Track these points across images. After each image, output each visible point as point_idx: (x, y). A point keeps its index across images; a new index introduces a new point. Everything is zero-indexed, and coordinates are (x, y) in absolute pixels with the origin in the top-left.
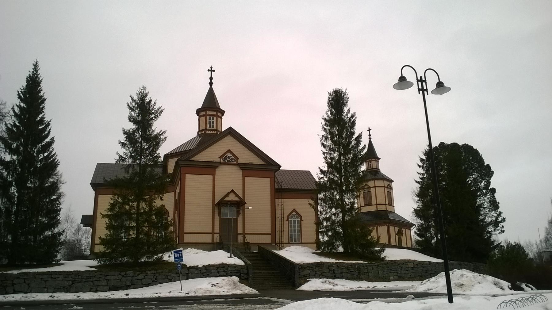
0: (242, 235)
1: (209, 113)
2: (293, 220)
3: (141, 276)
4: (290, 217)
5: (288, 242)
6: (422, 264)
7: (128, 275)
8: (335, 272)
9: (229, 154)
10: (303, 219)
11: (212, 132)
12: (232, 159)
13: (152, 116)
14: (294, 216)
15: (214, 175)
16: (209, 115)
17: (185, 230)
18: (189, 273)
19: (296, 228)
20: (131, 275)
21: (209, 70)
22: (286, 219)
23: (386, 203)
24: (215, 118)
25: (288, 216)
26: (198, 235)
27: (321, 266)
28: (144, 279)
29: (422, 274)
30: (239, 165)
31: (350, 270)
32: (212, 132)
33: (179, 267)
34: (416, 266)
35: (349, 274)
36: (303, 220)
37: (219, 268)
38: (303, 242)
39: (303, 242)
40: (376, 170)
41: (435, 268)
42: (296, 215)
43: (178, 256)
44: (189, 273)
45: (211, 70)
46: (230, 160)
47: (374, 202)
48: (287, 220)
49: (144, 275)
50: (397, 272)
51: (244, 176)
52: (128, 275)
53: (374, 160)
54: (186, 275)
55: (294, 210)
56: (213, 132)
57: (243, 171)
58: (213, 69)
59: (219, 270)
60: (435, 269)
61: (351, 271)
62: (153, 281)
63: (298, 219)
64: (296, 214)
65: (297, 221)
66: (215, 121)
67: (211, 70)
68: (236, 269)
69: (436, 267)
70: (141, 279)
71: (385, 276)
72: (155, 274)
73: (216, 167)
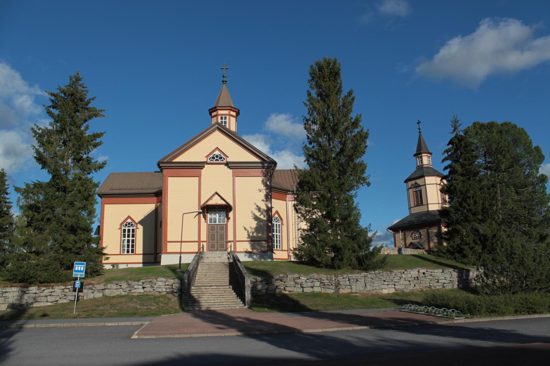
0: (232, 243)
1: (220, 112)
3: (47, 292)
6: (431, 272)
7: (31, 292)
8: (302, 286)
9: (217, 153)
12: (221, 158)
15: (199, 176)
16: (220, 115)
18: (105, 289)
20: (34, 292)
23: (438, 200)
24: (227, 117)
25: (121, 224)
27: (284, 279)
28: (50, 295)
29: (431, 285)
30: (227, 164)
31: (324, 283)
33: (78, 284)
34: (422, 275)
35: (323, 288)
37: (145, 283)
38: (136, 253)
39: (136, 253)
40: (428, 166)
41: (451, 276)
42: (131, 222)
43: (79, 269)
44: (105, 289)
46: (218, 159)
47: (424, 203)
49: (51, 290)
50: (394, 283)
51: (235, 175)
52: (31, 292)
54: (101, 291)
57: (233, 172)
59: (144, 286)
60: (451, 277)
61: (326, 284)
62: (60, 298)
63: (133, 227)
64: (131, 221)
66: (227, 120)
67: (419, 123)
68: (167, 283)
69: (451, 275)
70: (47, 296)
71: (376, 289)
72: (64, 289)
73: (202, 168)
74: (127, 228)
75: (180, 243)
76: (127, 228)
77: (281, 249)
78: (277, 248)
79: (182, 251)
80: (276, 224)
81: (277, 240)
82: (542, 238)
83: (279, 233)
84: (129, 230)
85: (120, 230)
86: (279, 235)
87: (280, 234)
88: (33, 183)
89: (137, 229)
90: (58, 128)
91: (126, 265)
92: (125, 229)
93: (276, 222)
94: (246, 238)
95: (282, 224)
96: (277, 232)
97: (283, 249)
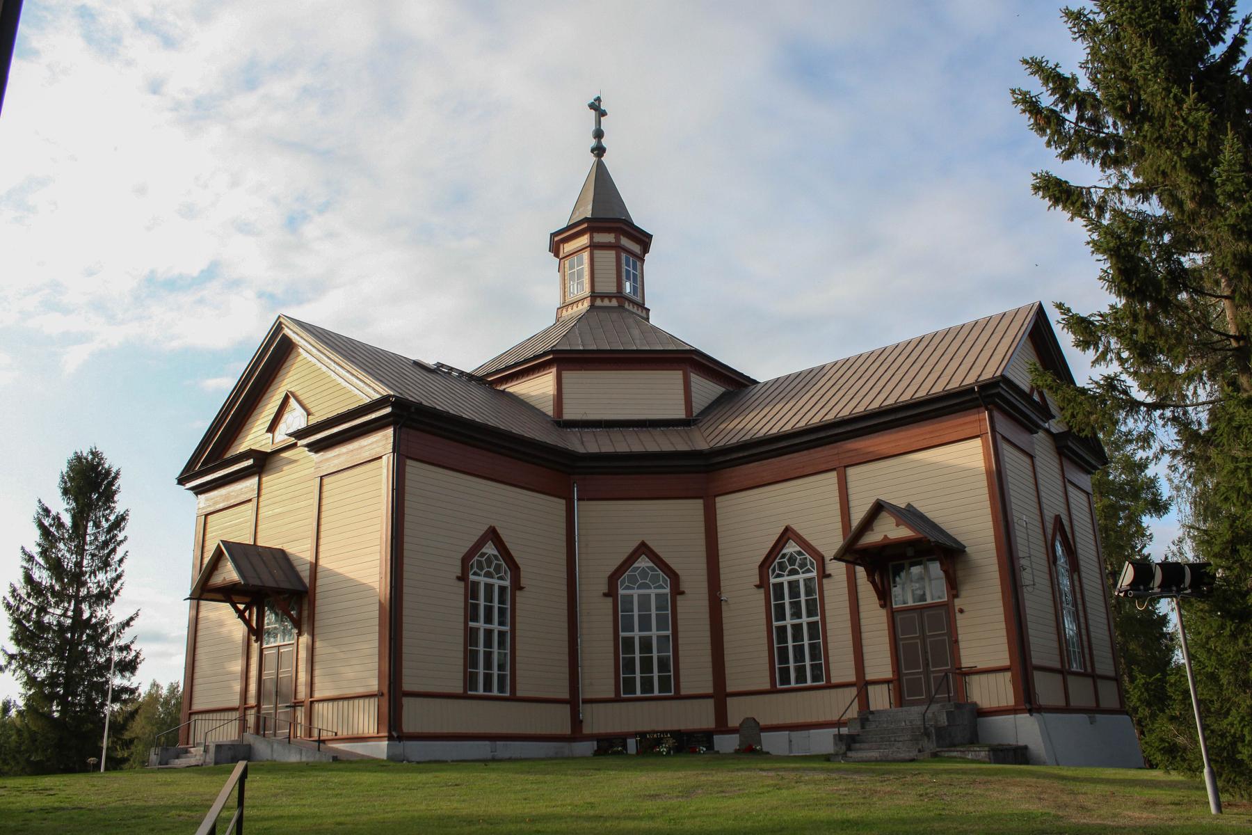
2: (785, 580)
4: (774, 571)
5: (612, 695)
10: (827, 572)
13: (1244, 211)
14: (644, 573)
17: (403, 685)
19: (651, 630)
21: (592, 106)
22: (758, 583)
25: (614, 578)
26: (444, 701)
36: (829, 576)
38: (683, 692)
42: (799, 553)
45: (596, 106)
48: (611, 593)
55: (643, 549)
56: (636, 308)
63: (661, 587)
64: (651, 564)
65: (657, 595)
76: (785, 580)
77: (507, 694)
78: (488, 686)
80: (489, 588)
81: (488, 656)
83: (501, 623)
85: (610, 600)
86: (502, 634)
87: (507, 628)
88: (79, 454)
89: (825, 581)
90: (1105, 257)
91: (499, 755)
92: (781, 584)
93: (488, 575)
95: (677, 591)
96: (488, 619)
97: (519, 694)
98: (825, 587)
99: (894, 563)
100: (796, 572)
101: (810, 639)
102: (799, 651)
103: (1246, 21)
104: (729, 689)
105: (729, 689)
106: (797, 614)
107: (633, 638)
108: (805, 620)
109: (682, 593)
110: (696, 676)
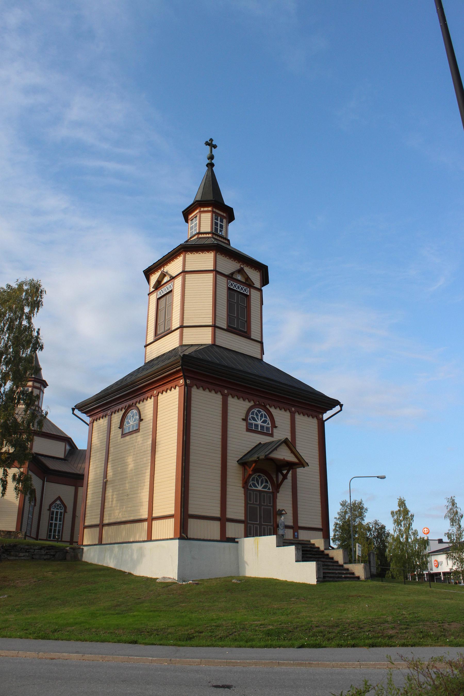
11: (22, 406)
21: (207, 144)
25: (50, 506)
32: (22, 406)
38: (63, 540)
39: (63, 540)
42: (60, 504)
45: (211, 144)
53: (206, 209)
58: (214, 143)
63: (61, 510)
64: (60, 503)
74: (55, 510)
75: (217, 514)
76: (55, 510)
79: (69, 540)
82: (106, 695)
83: (60, 521)
84: (57, 512)
94: (279, 508)
95: (65, 511)
98: (65, 515)
99: (262, 522)
100: (58, 509)
101: (54, 527)
102: (55, 530)
103: (39, 329)
104: (74, 541)
105: (74, 541)
106: (56, 520)
107: (53, 523)
108: (58, 522)
109: (67, 512)
110: (66, 536)
